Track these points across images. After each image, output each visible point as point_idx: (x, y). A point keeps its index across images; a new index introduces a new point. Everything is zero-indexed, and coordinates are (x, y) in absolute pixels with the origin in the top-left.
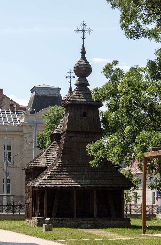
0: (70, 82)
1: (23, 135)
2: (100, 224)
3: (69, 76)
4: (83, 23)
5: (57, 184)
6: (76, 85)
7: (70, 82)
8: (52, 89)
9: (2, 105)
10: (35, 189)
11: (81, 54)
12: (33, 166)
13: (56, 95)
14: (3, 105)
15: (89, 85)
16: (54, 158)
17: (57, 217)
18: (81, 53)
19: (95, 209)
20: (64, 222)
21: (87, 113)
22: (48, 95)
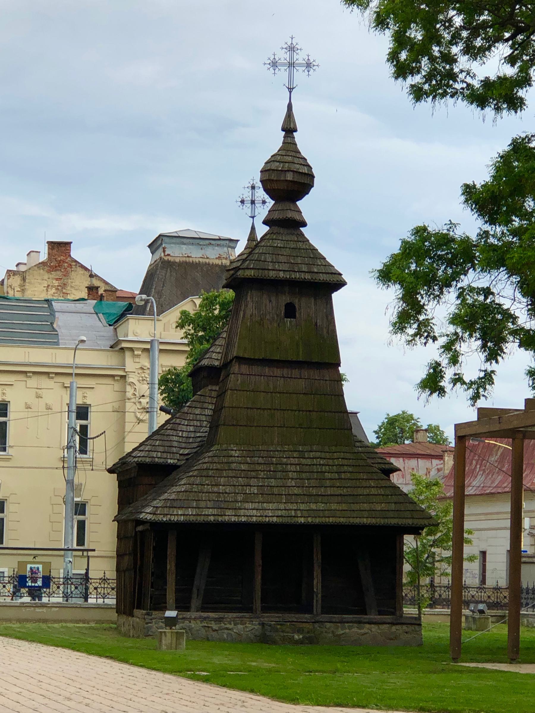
0: (253, 217)
1: (123, 377)
2: (331, 635)
3: (248, 199)
4: (289, 44)
5: (203, 513)
6: (265, 222)
7: (251, 217)
8: (213, 242)
9: (69, 288)
10: (140, 528)
11: (284, 133)
12: (136, 460)
13: (224, 261)
14: (69, 290)
15: (304, 224)
16: (199, 439)
17: (253, 603)
18: (283, 130)
19: (317, 589)
20: (225, 624)
21: (297, 306)
22: (201, 260)
